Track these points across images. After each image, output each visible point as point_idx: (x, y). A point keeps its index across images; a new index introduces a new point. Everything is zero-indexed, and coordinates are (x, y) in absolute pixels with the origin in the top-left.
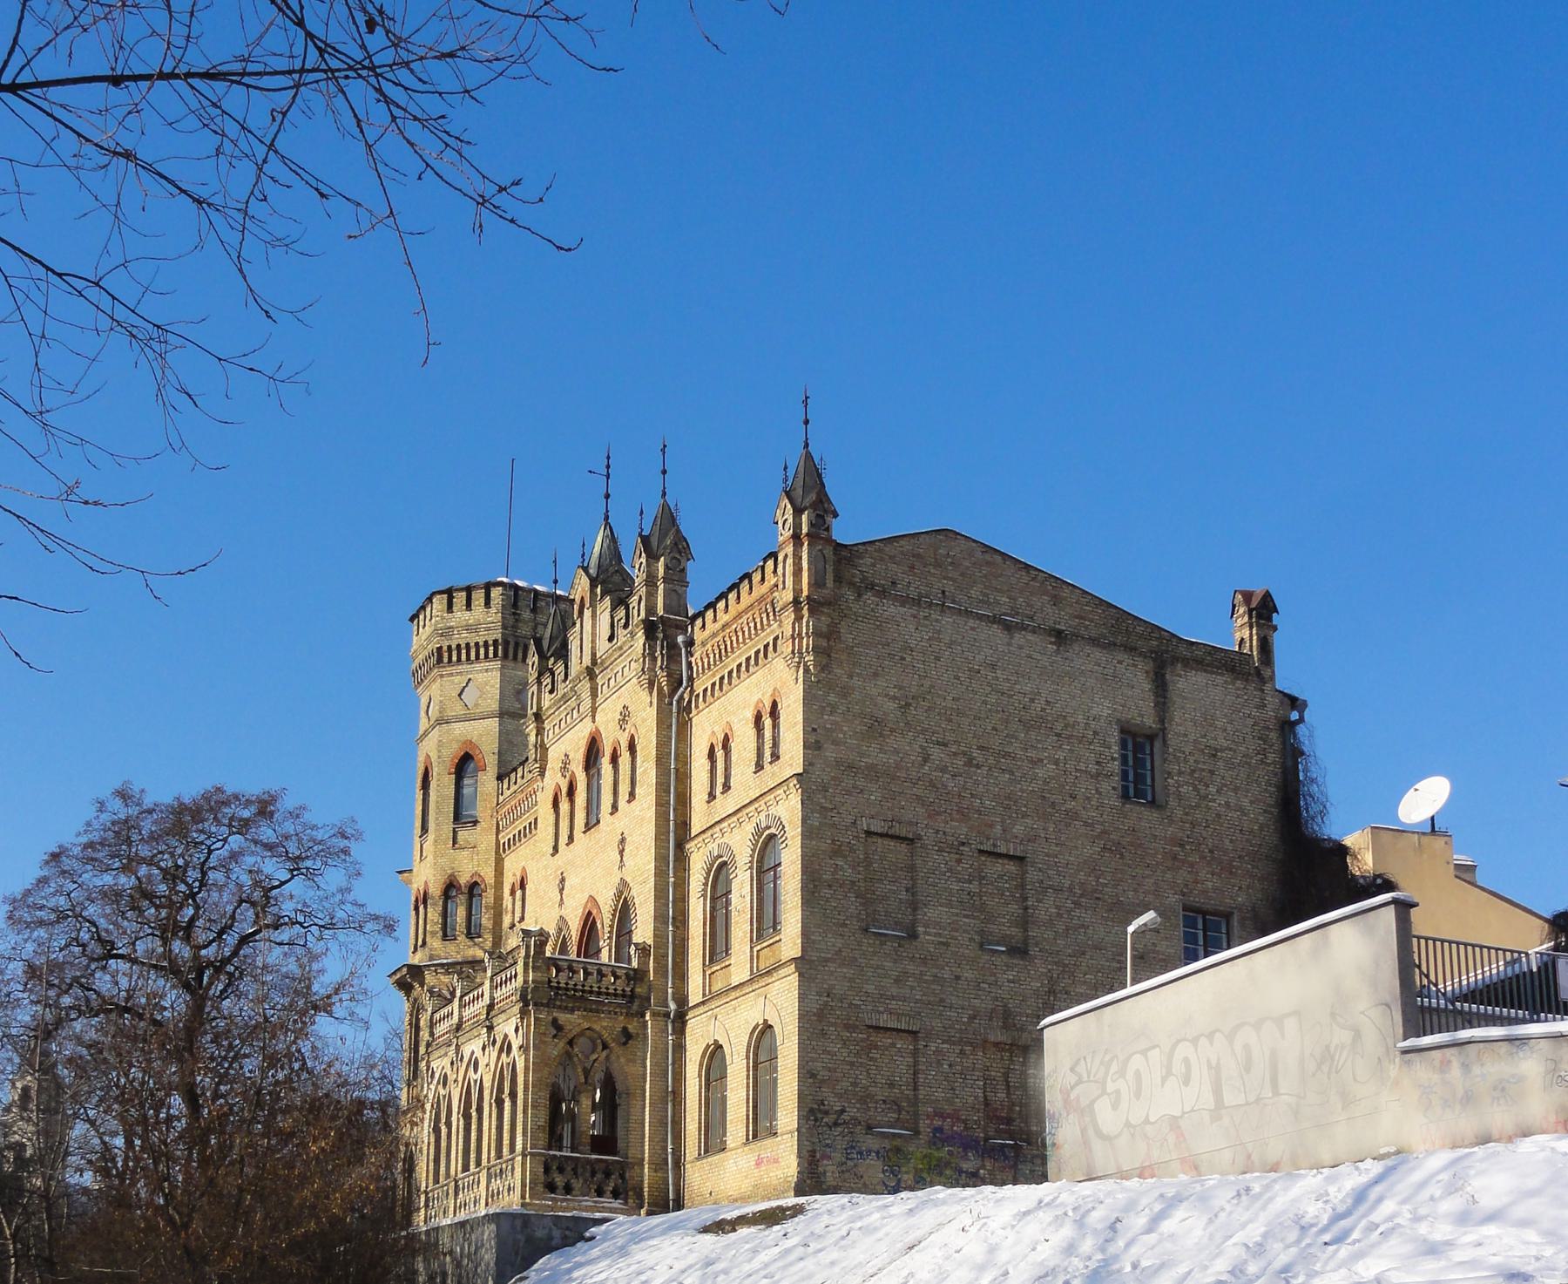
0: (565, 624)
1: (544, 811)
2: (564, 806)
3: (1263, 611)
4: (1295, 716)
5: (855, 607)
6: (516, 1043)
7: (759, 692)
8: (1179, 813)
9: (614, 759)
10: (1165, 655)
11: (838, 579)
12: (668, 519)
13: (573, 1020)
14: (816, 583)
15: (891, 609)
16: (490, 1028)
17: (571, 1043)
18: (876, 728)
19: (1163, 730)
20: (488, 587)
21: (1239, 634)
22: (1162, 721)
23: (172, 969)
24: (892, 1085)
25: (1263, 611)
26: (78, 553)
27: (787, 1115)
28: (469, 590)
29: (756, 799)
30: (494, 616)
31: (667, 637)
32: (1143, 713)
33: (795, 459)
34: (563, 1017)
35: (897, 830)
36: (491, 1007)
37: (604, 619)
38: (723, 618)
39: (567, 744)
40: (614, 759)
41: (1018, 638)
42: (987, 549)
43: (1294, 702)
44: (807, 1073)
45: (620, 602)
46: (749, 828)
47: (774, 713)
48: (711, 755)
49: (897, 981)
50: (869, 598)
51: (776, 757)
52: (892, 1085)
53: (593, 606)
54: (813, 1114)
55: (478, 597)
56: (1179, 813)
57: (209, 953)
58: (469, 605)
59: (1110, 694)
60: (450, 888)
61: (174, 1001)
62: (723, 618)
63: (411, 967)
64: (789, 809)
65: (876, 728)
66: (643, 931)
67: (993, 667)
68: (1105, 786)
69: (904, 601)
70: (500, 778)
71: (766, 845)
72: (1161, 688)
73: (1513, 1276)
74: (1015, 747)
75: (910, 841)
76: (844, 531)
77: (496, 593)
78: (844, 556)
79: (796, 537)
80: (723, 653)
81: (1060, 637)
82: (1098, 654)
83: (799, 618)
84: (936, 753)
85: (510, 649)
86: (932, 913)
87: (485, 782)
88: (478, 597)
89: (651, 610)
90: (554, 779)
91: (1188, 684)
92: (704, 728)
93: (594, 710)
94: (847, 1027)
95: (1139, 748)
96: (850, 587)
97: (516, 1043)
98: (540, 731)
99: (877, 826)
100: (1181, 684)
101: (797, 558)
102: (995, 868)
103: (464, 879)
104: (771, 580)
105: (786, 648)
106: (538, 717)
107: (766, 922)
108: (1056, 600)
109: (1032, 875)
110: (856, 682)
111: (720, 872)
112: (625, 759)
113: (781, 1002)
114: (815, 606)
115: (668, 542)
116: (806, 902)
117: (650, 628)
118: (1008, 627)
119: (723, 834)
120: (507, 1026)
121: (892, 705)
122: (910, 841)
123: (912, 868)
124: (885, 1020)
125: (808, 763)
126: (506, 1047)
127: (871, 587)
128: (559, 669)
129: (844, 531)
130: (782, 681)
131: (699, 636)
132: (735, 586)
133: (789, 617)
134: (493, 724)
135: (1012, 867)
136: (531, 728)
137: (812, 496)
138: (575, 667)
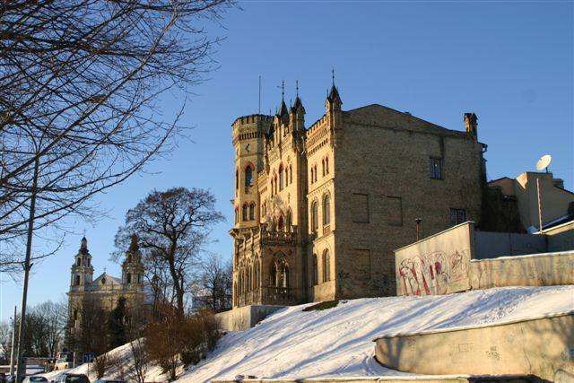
0: (272, 130)
1: (269, 185)
2: (274, 183)
3: (472, 119)
4: (484, 149)
5: (349, 129)
6: (259, 255)
7: (322, 154)
8: (448, 181)
9: (286, 171)
10: (442, 134)
11: (344, 122)
12: (298, 102)
13: (275, 249)
14: (337, 123)
15: (360, 129)
16: (253, 251)
17: (274, 255)
18: (356, 163)
19: (443, 158)
20: (253, 116)
21: (463, 126)
22: (442, 154)
23: (166, 233)
24: (363, 265)
25: (472, 119)
26: (124, 175)
27: (333, 275)
28: (248, 117)
29: (323, 186)
30: (255, 125)
31: (299, 135)
32: (436, 152)
33: (330, 89)
34: (272, 248)
35: (363, 192)
36: (253, 245)
37: (283, 130)
38: (314, 132)
39: (274, 166)
40: (286, 171)
41: (398, 134)
42: (388, 109)
43: (484, 146)
44: (337, 264)
45: (286, 126)
46: (322, 193)
47: (327, 160)
48: (312, 171)
49: (364, 236)
50: (353, 126)
51: (328, 172)
52: (363, 265)
53: (280, 126)
54: (339, 275)
55: (251, 119)
56: (448, 181)
57: (177, 229)
58: (248, 122)
59: (424, 148)
60: (245, 207)
61: (167, 242)
62: (314, 132)
63: (234, 230)
64: (331, 188)
65: (356, 163)
66: (295, 222)
67: (390, 143)
68: (426, 175)
69: (364, 126)
70: (258, 173)
71: (326, 198)
72: (442, 145)
73: (297, 381)
74: (397, 166)
75: (367, 195)
76: (344, 108)
77: (255, 118)
78: (346, 114)
79: (331, 111)
80: (314, 141)
81: (411, 132)
82: (423, 136)
83: (332, 134)
84: (374, 169)
85: (259, 135)
86: (373, 215)
87: (254, 174)
88: (251, 119)
89: (295, 129)
90: (271, 175)
91: (449, 143)
92: (311, 161)
93: (281, 156)
94: (350, 250)
95: (438, 160)
96: (346, 124)
97: (259, 255)
98: (267, 161)
99: (357, 192)
100: (449, 143)
101: (332, 117)
102: (392, 201)
103: (249, 203)
104: (325, 122)
105: (329, 142)
106: (267, 157)
107: (325, 221)
108: (409, 122)
109: (404, 203)
110: (349, 151)
111: (315, 204)
112: (289, 171)
113: (331, 239)
114: (337, 130)
115: (298, 108)
116: (336, 215)
117: (294, 134)
118: (395, 131)
119: (315, 195)
120: (257, 250)
121: (360, 157)
122: (367, 195)
123: (367, 204)
124: (360, 247)
125: (336, 175)
126: (257, 257)
127: (354, 123)
128: (271, 143)
129: (344, 108)
130: (328, 151)
131: (308, 137)
132: (316, 123)
133: (329, 133)
134: (256, 157)
135: (397, 200)
136: (265, 161)
137: (334, 97)
138: (276, 144)
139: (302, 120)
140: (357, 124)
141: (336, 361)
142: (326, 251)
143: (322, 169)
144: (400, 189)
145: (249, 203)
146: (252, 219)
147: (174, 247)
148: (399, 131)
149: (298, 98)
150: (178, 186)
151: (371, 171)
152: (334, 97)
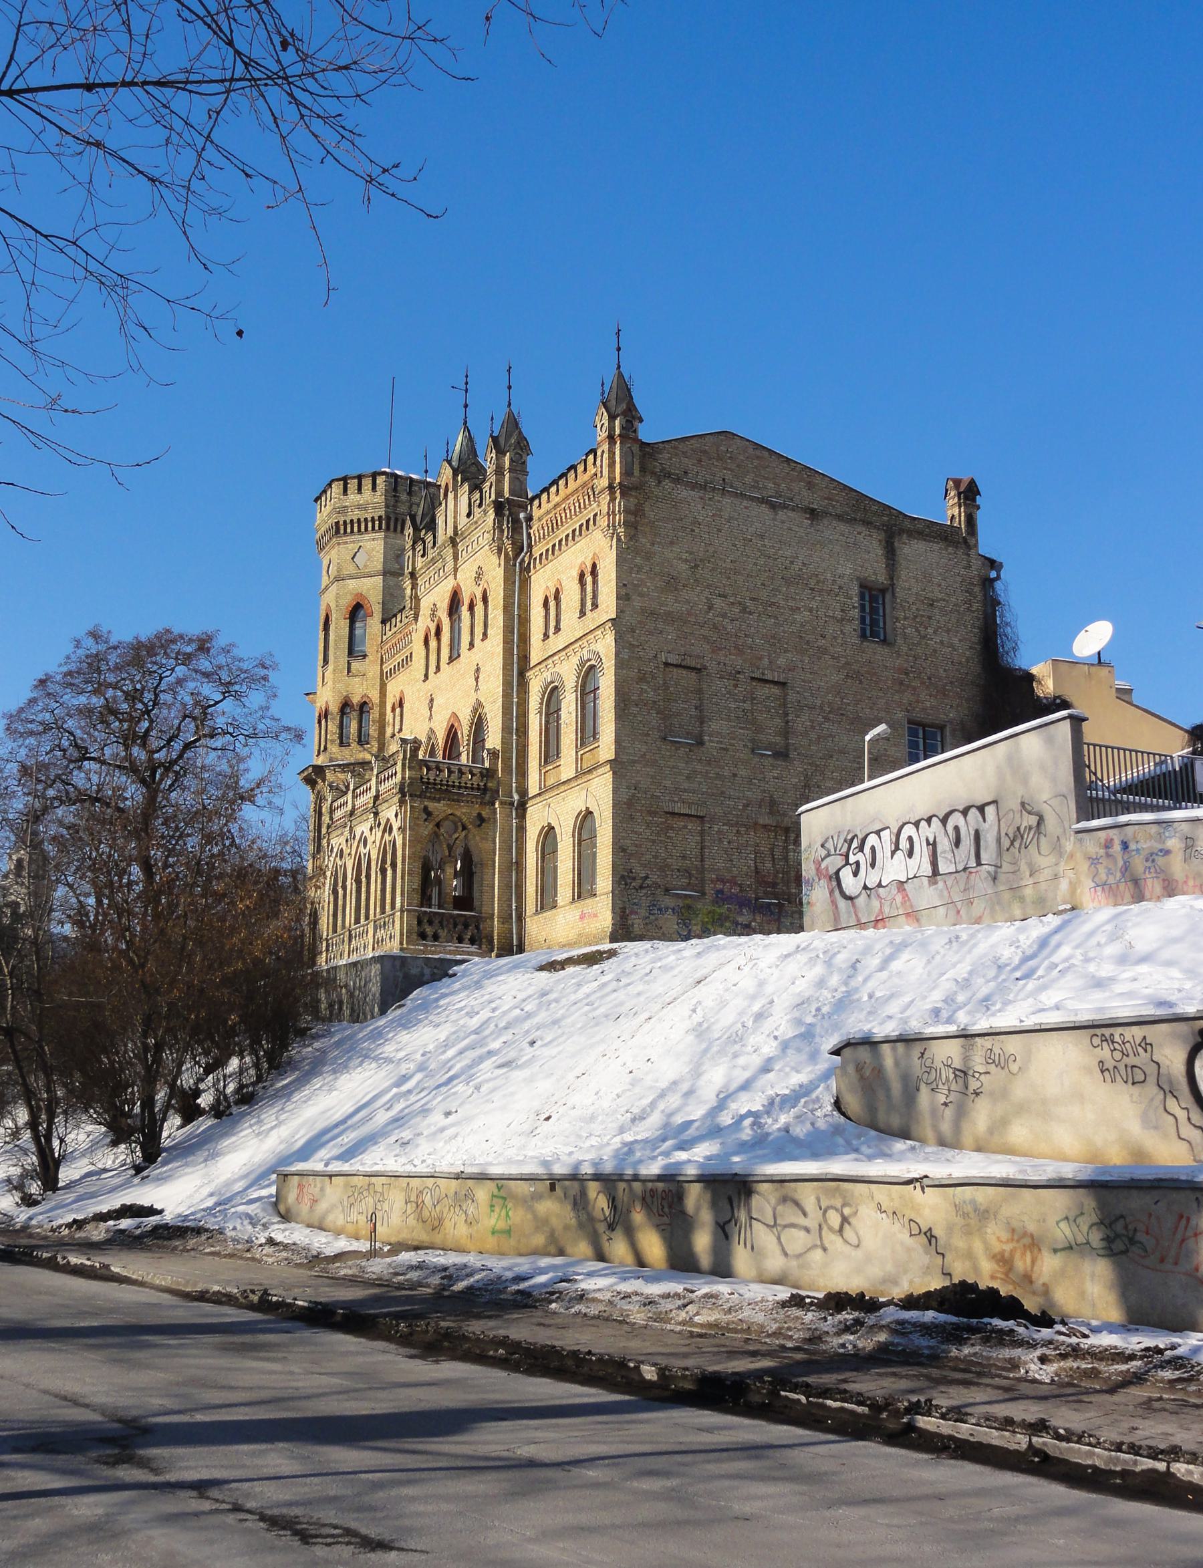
0: (433, 504)
1: (418, 648)
2: (433, 644)
3: (969, 494)
4: (993, 574)
6: (396, 825)
7: (582, 555)
8: (905, 649)
9: (471, 608)
10: (893, 527)
11: (643, 469)
12: (512, 423)
13: (439, 808)
14: (627, 473)
15: (684, 493)
16: (376, 814)
17: (438, 825)
18: (672, 584)
20: (374, 476)
21: (950, 511)
22: (892, 579)
23: (132, 768)
24: (684, 857)
25: (969, 494)
26: (60, 449)
27: (604, 881)
28: (360, 478)
29: (580, 639)
30: (379, 498)
31: (512, 514)
32: (877, 572)
33: (610, 378)
34: (432, 805)
35: (688, 662)
36: (376, 798)
37: (464, 500)
38: (555, 499)
39: (435, 596)
40: (471, 608)
41: (781, 514)
43: (993, 564)
44: (619, 849)
45: (476, 487)
46: (575, 660)
47: (594, 572)
50: (667, 484)
51: (595, 606)
52: (684, 857)
53: (455, 490)
54: (623, 879)
55: (367, 483)
56: (905, 649)
57: (160, 756)
58: (360, 490)
59: (851, 558)
60: (345, 706)
61: (134, 793)
62: (555, 499)
64: (605, 646)
65: (672, 584)
66: (494, 740)
67: (762, 537)
68: (848, 628)
69: (694, 486)
70: (384, 622)
71: (588, 674)
72: (891, 553)
75: (698, 670)
76: (647, 433)
77: (380, 480)
79: (611, 438)
80: (555, 526)
81: (813, 514)
82: (842, 527)
83: (613, 499)
84: (718, 603)
87: (372, 626)
88: (367, 483)
89: (499, 493)
90: (425, 623)
91: (912, 550)
92: (540, 584)
93: (456, 570)
94: (650, 813)
96: (652, 475)
97: (396, 825)
98: (414, 586)
99: (673, 659)
100: (906, 550)
101: (612, 453)
102: (764, 691)
103: (356, 700)
104: (591, 470)
105: (603, 522)
106: (413, 575)
107: (587, 733)
108: (810, 486)
109: (792, 696)
111: (552, 694)
112: (479, 608)
113: (599, 794)
114: (626, 490)
115: (512, 441)
117: (499, 507)
118: (773, 506)
120: (389, 812)
121: (685, 566)
122: (698, 670)
123: (700, 691)
124: (679, 808)
125: (620, 611)
126: (388, 828)
127: (668, 475)
128: (429, 538)
129: (647, 433)
130: (600, 548)
131: (536, 513)
132: (564, 475)
133: (605, 498)
135: (776, 690)
137: (623, 405)
138: (441, 537)
139: (519, 468)
140: (677, 481)
141: (284, 1132)
142: (587, 816)
143: (541, 621)
144: (781, 661)
145: (356, 700)
146: (362, 741)
147: (151, 805)
148: (785, 507)
149: (510, 414)
150: (190, 626)
151: (710, 608)
152: (623, 405)
